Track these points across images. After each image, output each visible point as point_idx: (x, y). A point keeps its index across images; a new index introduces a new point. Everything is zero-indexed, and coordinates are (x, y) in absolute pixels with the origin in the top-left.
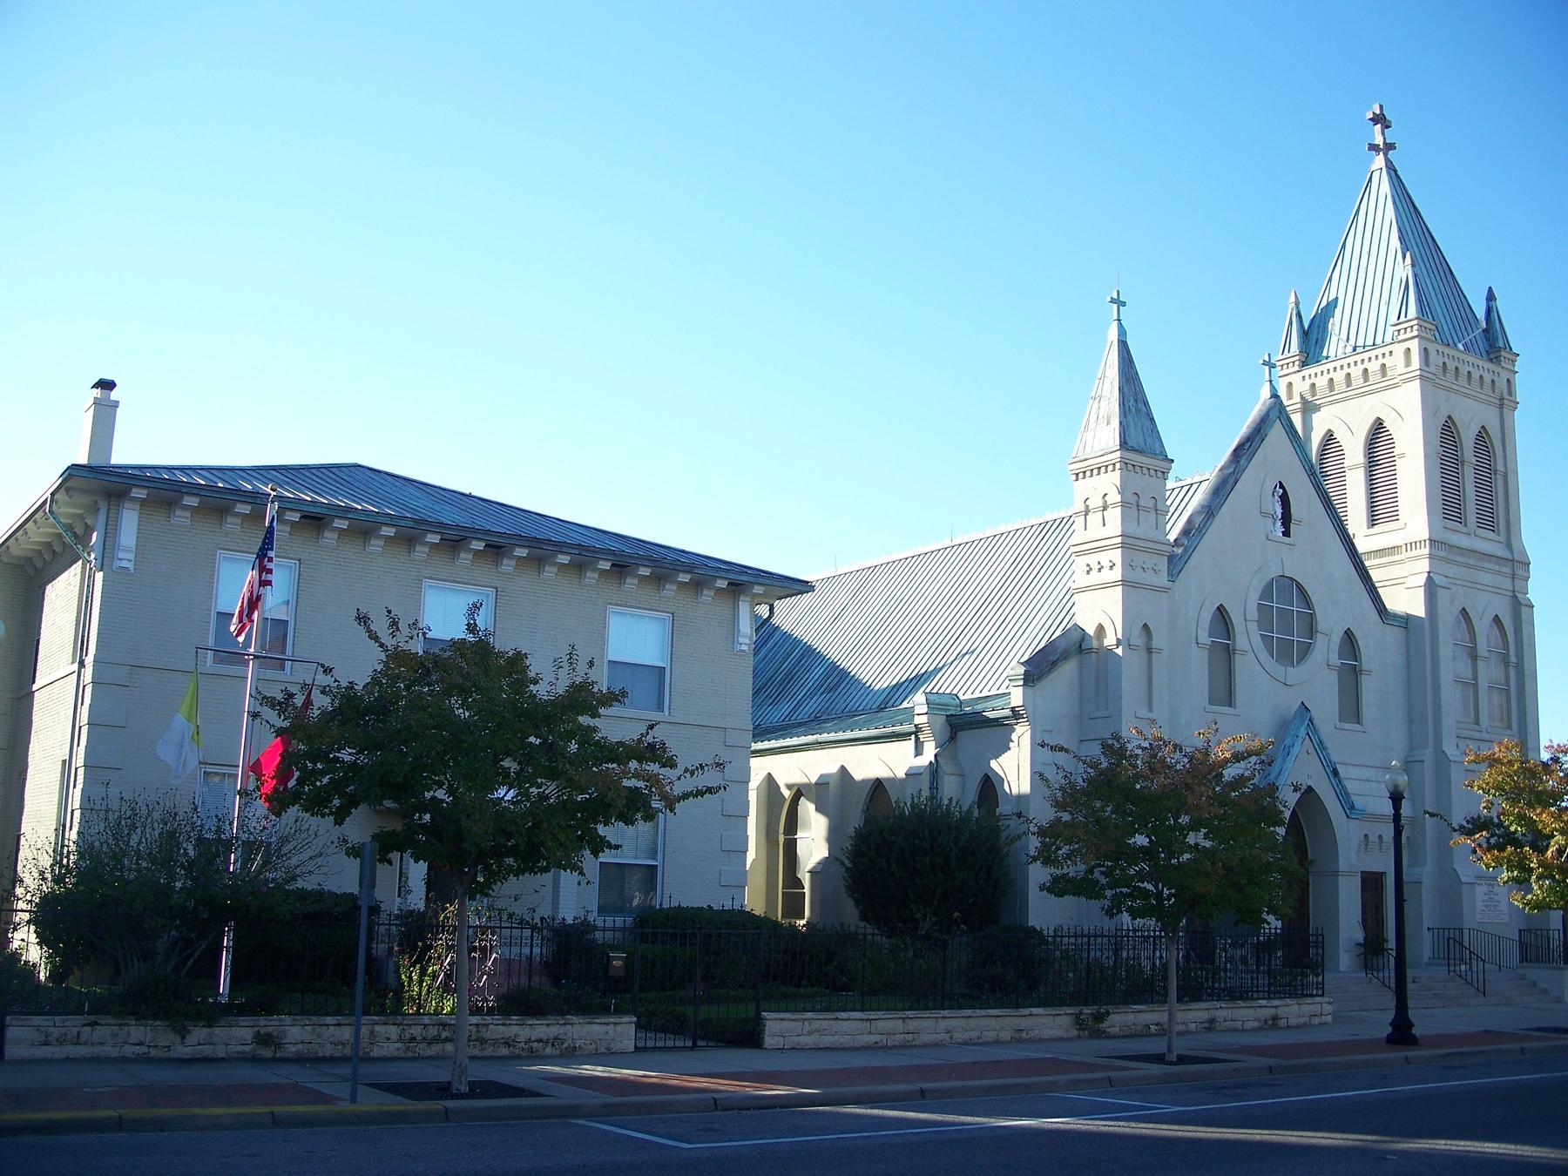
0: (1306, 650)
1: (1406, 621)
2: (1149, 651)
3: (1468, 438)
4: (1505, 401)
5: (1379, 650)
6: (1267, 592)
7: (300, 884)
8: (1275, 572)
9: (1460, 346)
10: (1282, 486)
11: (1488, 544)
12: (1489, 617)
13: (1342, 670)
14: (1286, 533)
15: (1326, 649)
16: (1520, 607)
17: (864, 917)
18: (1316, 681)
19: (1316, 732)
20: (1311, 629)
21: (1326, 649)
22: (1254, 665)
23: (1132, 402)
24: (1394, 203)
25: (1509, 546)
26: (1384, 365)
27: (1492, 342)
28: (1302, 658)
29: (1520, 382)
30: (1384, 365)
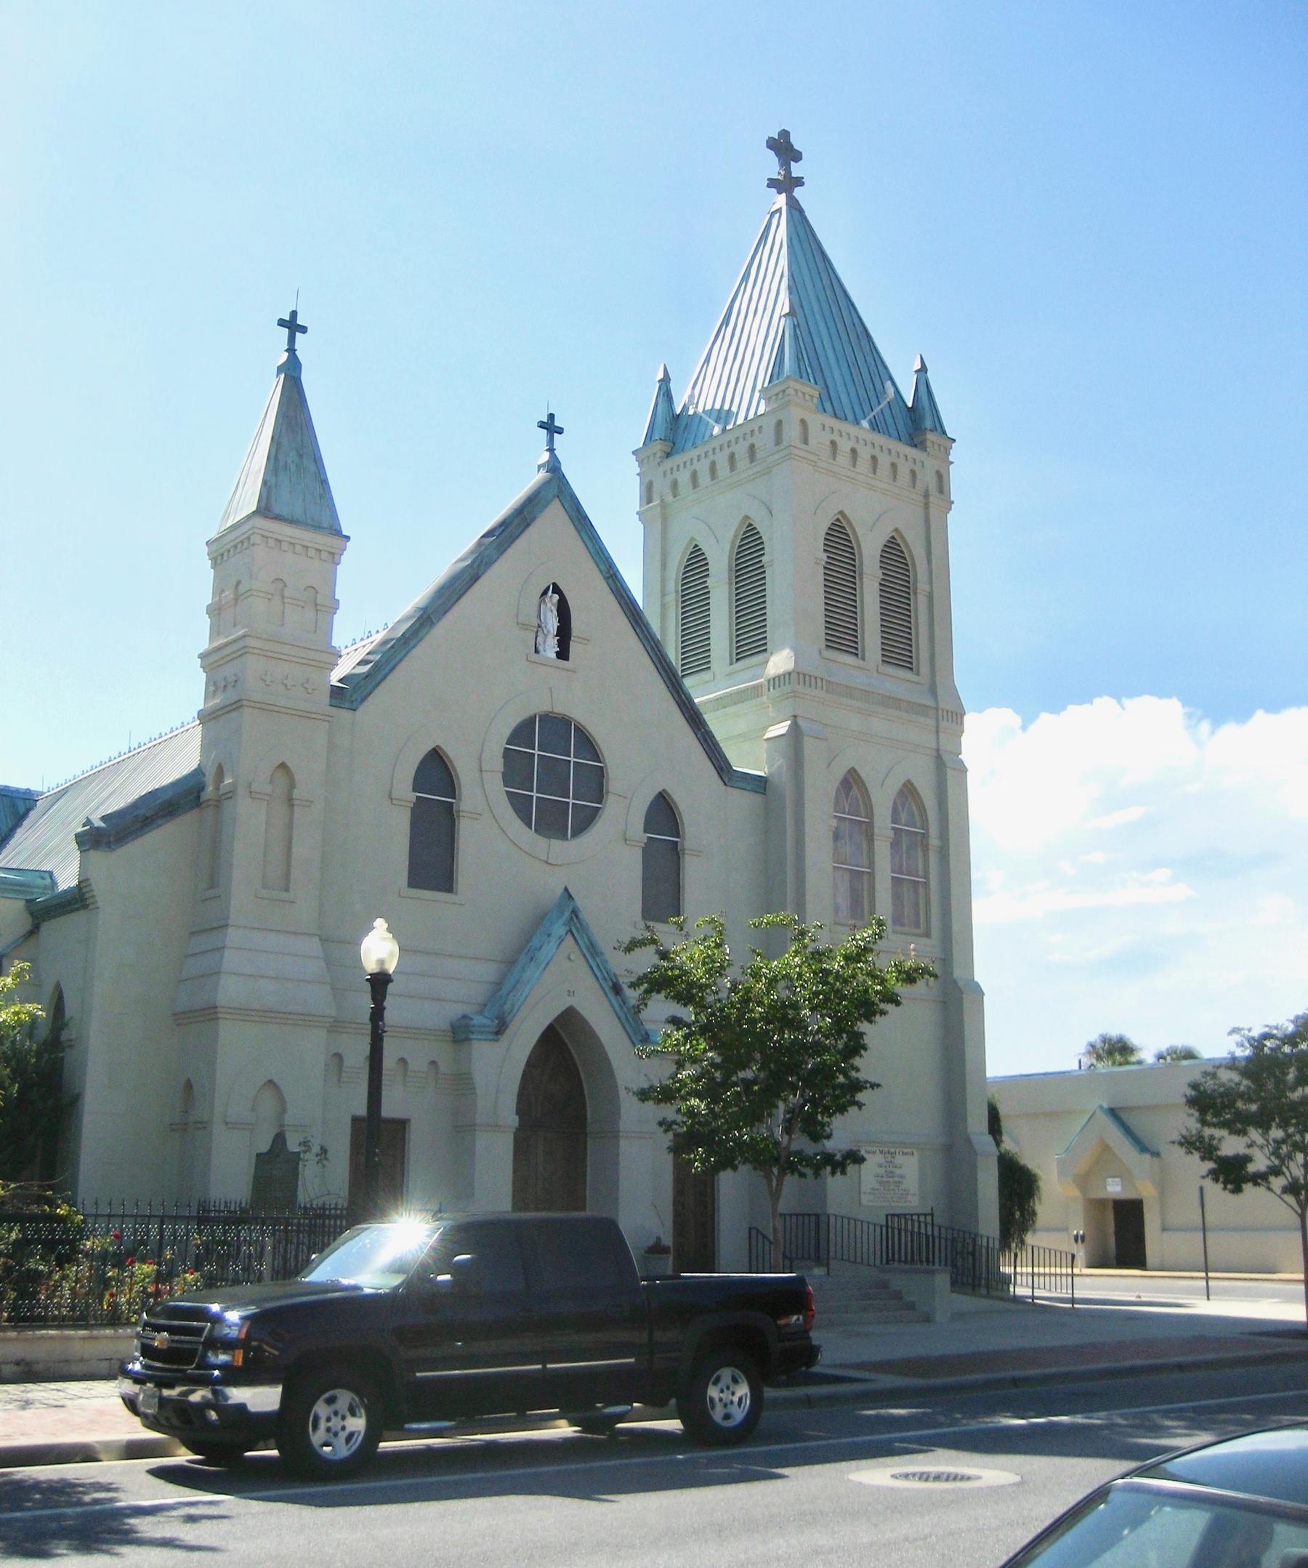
0: (586, 820)
1: (759, 785)
2: (290, 802)
3: (870, 549)
4: (935, 495)
5: (713, 825)
6: (523, 732)
7: (118, 1504)
8: (540, 705)
9: (865, 424)
10: (557, 590)
11: (896, 682)
12: (894, 785)
13: (649, 850)
14: (563, 654)
15: (623, 817)
16: (947, 769)
17: (207, 1308)
18: (604, 863)
19: (583, 928)
20: (599, 793)
21: (623, 817)
22: (489, 826)
23: (293, 456)
24: (790, 246)
25: (933, 690)
26: (752, 446)
27: (918, 423)
28: (580, 829)
29: (957, 476)
30: (752, 446)
